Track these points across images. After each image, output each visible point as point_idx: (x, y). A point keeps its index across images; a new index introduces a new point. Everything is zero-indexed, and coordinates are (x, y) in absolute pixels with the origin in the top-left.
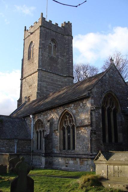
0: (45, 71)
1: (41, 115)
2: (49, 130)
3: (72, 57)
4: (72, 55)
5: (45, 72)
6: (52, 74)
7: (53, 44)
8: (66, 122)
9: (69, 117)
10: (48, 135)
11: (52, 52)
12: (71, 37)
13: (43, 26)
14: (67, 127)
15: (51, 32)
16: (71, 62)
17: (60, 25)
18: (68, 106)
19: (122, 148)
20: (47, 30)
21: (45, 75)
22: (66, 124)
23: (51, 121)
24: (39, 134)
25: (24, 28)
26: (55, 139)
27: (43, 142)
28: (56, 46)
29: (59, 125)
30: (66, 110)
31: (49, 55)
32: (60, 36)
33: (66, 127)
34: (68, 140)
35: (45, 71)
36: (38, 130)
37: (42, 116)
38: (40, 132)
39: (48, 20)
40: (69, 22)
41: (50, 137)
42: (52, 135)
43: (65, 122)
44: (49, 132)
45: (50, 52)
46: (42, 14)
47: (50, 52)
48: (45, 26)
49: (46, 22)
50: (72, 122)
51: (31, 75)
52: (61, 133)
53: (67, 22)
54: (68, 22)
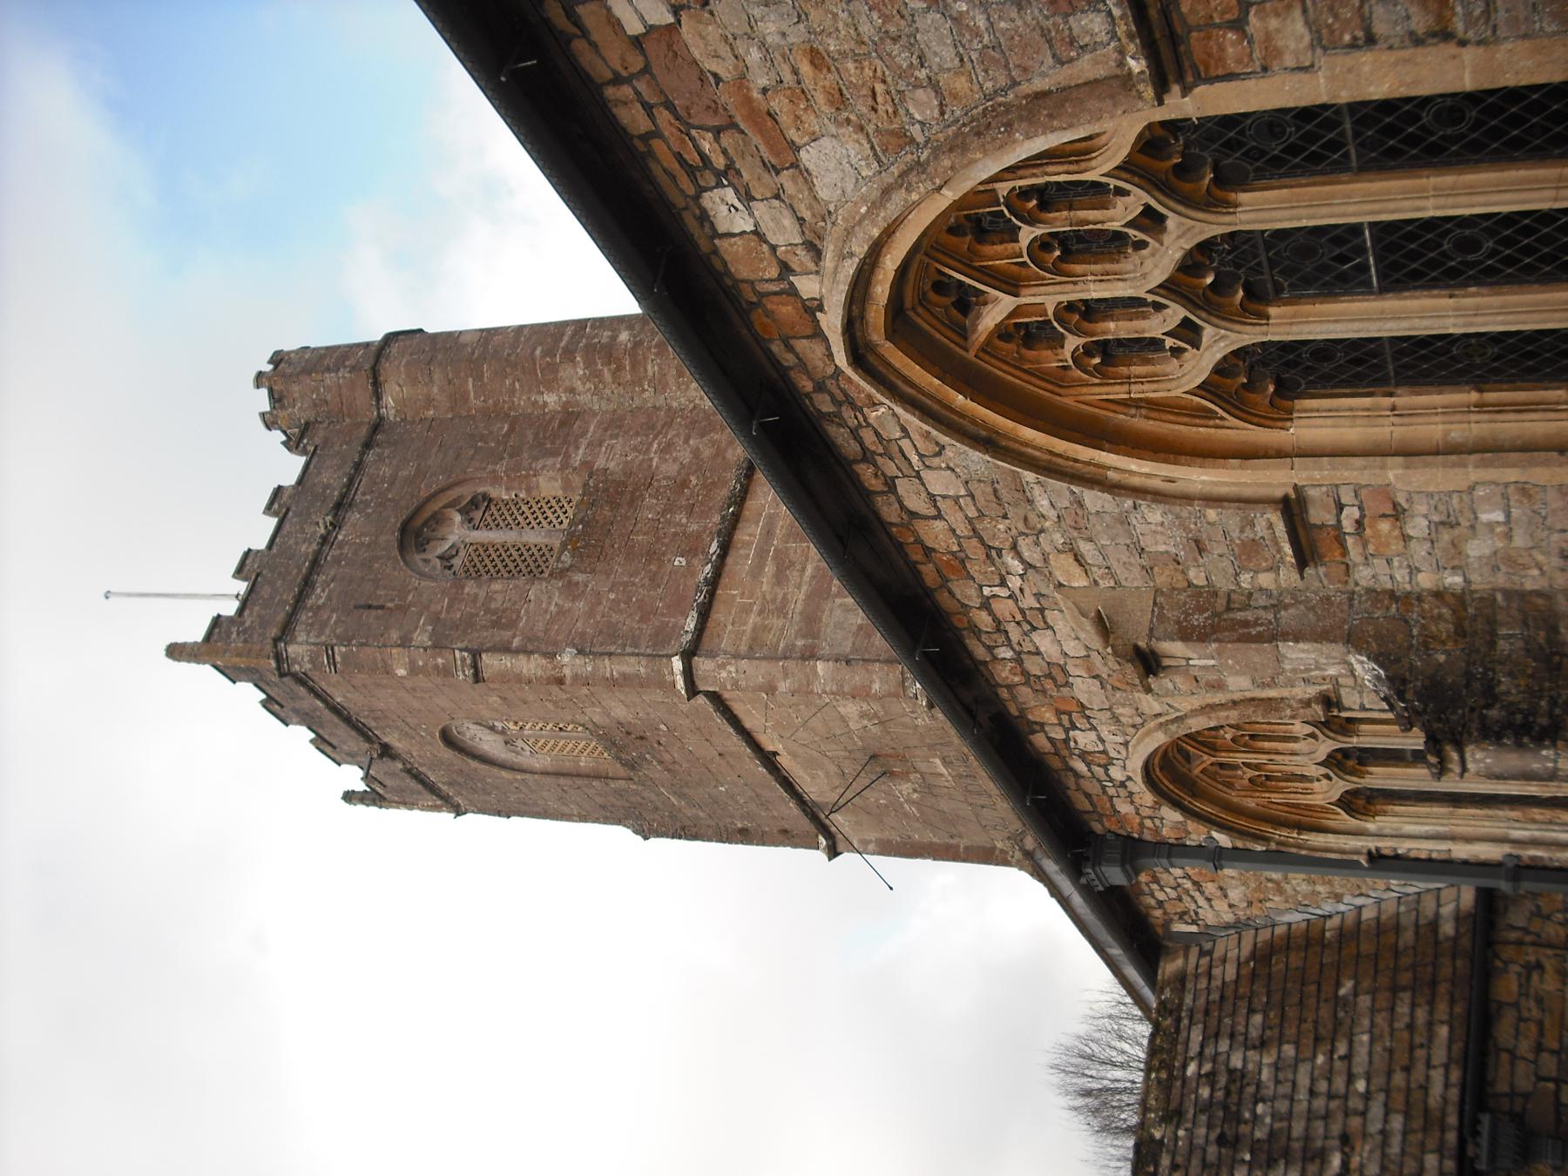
0: (705, 614)
1: (1084, 755)
2: (1297, 654)
3: (581, 325)
4: (565, 324)
5: (719, 615)
6: (741, 536)
7: (457, 532)
8: (1114, 329)
9: (1011, 285)
10: (1397, 684)
11: (533, 537)
12: (394, 349)
13: (276, 640)
14: (1210, 303)
15: (337, 561)
16: (624, 336)
17: (289, 468)
18: (786, 310)
19: (1145, 1158)
20: (319, 596)
21: (747, 610)
22: (1155, 326)
23: (1137, 625)
24: (1380, 777)
25: (361, 809)
26: (1477, 549)
27: (1528, 777)
28: (474, 503)
29: (1197, 477)
30: (859, 354)
31: (562, 573)
32: (381, 459)
33: (1218, 342)
34: (1492, 275)
35: (705, 614)
36: (1326, 791)
37: (1085, 740)
38: (1338, 762)
39: (226, 599)
40: (260, 375)
41: (1428, 641)
42: (1156, 93)
43: (1110, 353)
44: (1337, 649)
45: (529, 565)
46: (176, 652)
47: (529, 565)
48: (281, 617)
49: (245, 602)
50: (1097, 193)
51: (769, 760)
52: (1352, 434)
53: (262, 401)
54: (264, 392)
